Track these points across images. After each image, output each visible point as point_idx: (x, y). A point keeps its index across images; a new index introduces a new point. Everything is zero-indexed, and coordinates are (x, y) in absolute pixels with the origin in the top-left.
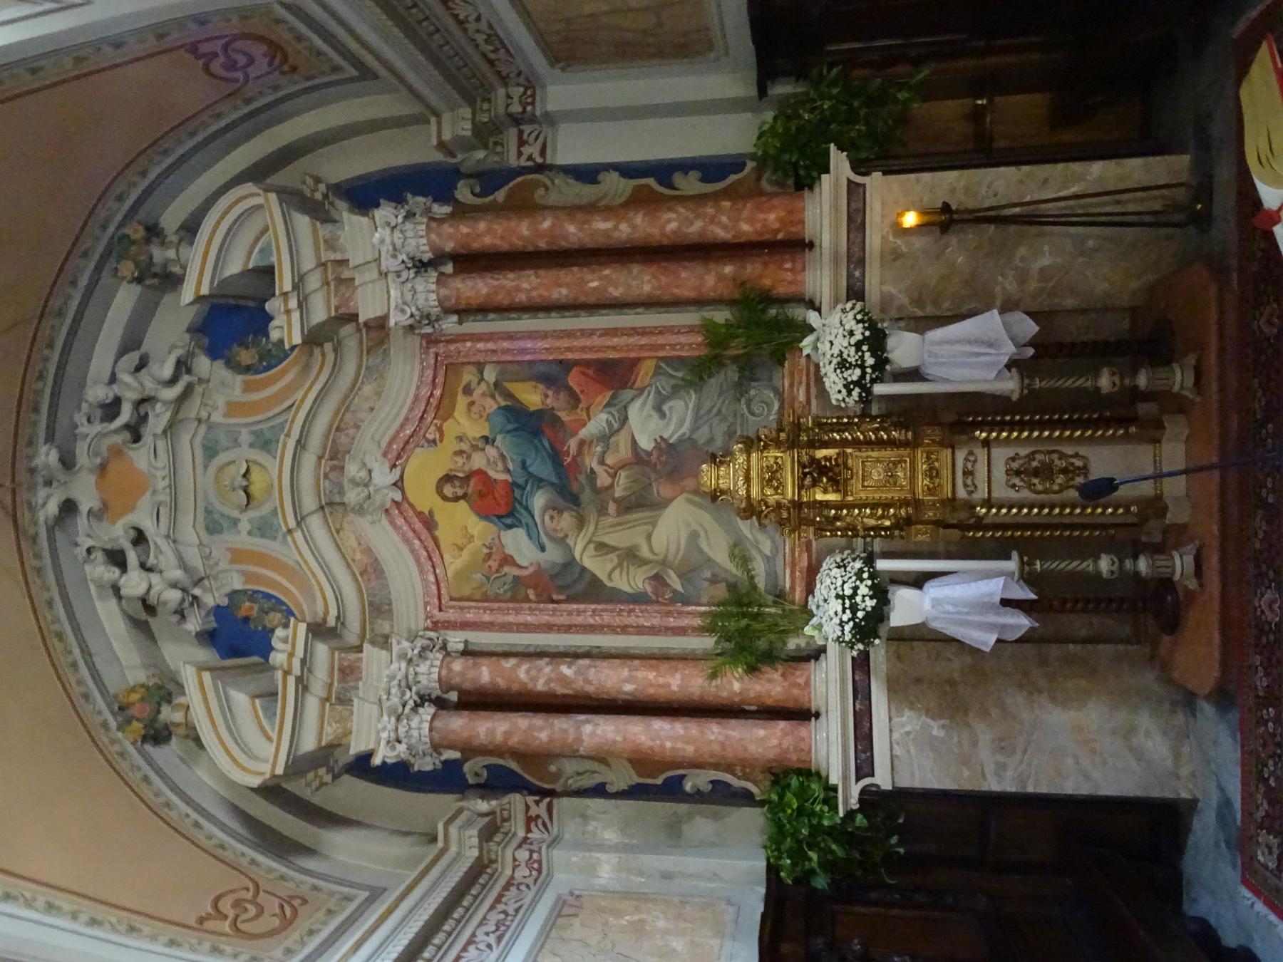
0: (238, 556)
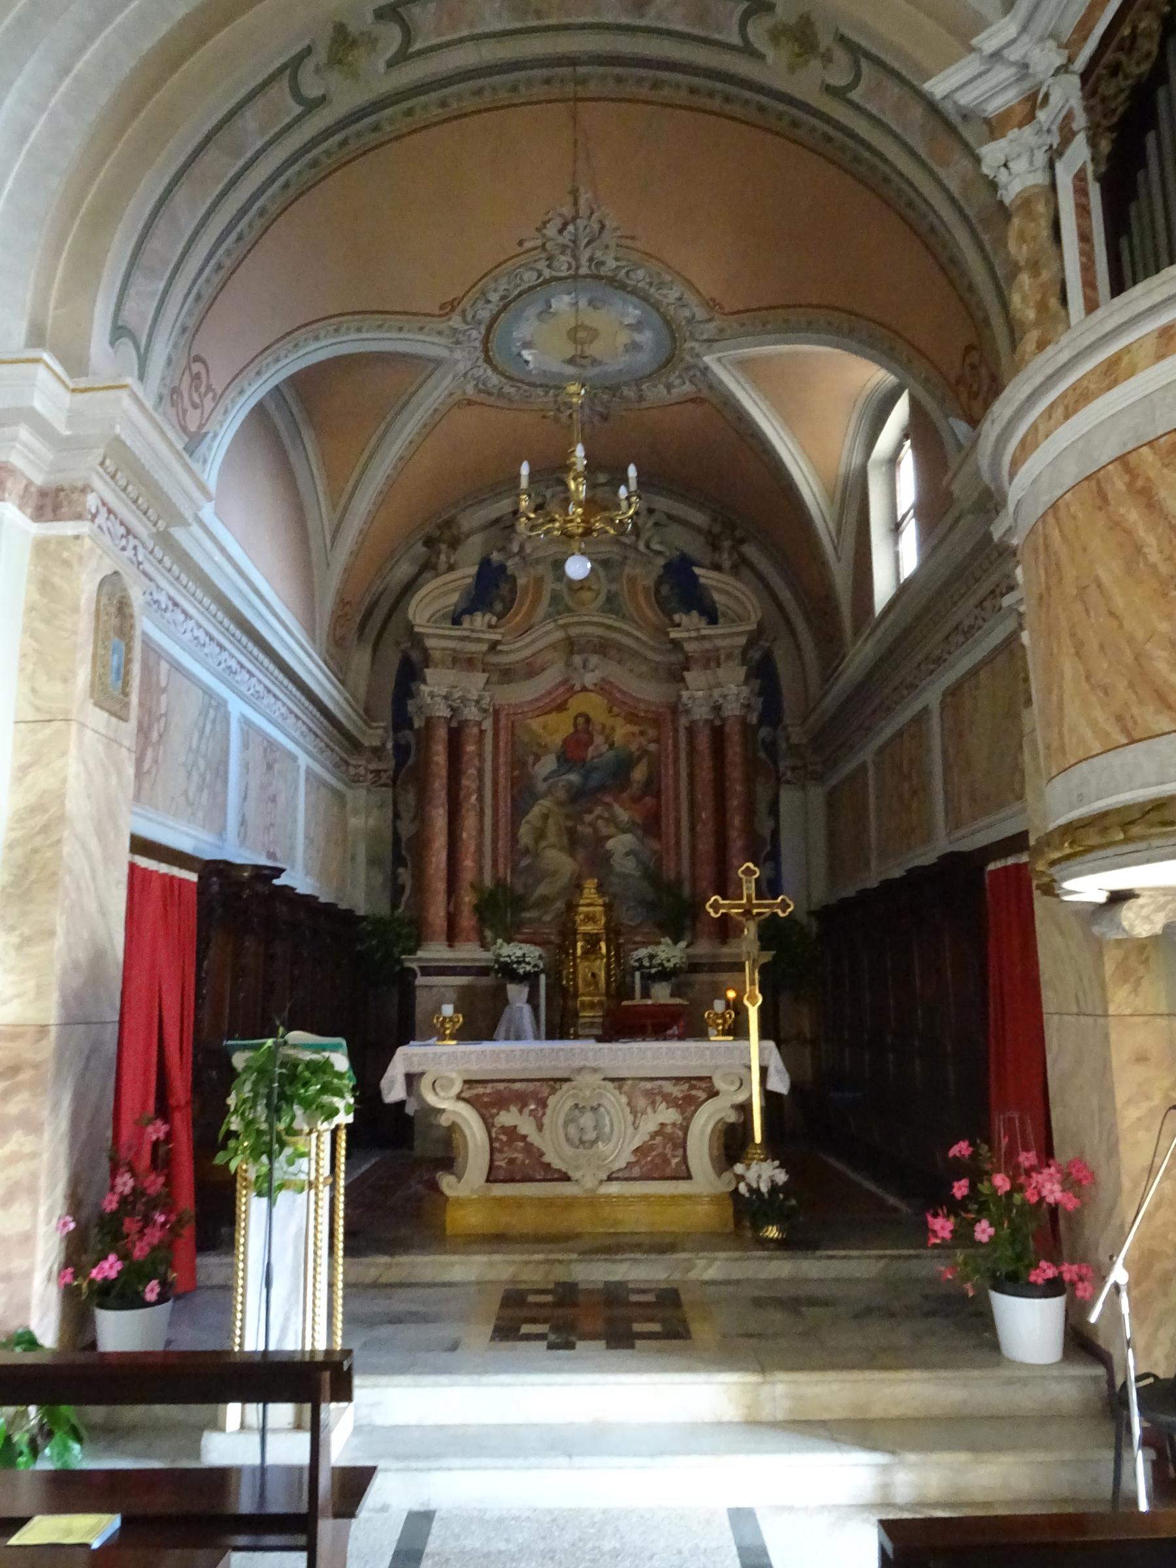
0: (539, 581)
